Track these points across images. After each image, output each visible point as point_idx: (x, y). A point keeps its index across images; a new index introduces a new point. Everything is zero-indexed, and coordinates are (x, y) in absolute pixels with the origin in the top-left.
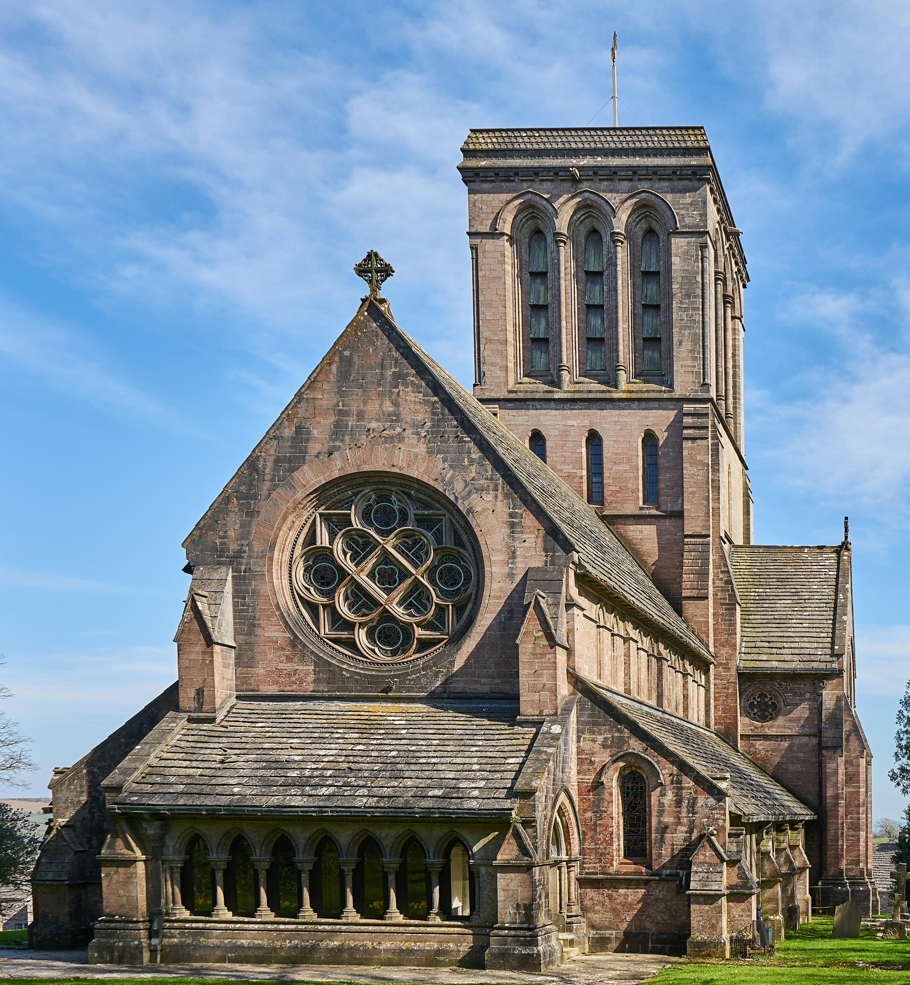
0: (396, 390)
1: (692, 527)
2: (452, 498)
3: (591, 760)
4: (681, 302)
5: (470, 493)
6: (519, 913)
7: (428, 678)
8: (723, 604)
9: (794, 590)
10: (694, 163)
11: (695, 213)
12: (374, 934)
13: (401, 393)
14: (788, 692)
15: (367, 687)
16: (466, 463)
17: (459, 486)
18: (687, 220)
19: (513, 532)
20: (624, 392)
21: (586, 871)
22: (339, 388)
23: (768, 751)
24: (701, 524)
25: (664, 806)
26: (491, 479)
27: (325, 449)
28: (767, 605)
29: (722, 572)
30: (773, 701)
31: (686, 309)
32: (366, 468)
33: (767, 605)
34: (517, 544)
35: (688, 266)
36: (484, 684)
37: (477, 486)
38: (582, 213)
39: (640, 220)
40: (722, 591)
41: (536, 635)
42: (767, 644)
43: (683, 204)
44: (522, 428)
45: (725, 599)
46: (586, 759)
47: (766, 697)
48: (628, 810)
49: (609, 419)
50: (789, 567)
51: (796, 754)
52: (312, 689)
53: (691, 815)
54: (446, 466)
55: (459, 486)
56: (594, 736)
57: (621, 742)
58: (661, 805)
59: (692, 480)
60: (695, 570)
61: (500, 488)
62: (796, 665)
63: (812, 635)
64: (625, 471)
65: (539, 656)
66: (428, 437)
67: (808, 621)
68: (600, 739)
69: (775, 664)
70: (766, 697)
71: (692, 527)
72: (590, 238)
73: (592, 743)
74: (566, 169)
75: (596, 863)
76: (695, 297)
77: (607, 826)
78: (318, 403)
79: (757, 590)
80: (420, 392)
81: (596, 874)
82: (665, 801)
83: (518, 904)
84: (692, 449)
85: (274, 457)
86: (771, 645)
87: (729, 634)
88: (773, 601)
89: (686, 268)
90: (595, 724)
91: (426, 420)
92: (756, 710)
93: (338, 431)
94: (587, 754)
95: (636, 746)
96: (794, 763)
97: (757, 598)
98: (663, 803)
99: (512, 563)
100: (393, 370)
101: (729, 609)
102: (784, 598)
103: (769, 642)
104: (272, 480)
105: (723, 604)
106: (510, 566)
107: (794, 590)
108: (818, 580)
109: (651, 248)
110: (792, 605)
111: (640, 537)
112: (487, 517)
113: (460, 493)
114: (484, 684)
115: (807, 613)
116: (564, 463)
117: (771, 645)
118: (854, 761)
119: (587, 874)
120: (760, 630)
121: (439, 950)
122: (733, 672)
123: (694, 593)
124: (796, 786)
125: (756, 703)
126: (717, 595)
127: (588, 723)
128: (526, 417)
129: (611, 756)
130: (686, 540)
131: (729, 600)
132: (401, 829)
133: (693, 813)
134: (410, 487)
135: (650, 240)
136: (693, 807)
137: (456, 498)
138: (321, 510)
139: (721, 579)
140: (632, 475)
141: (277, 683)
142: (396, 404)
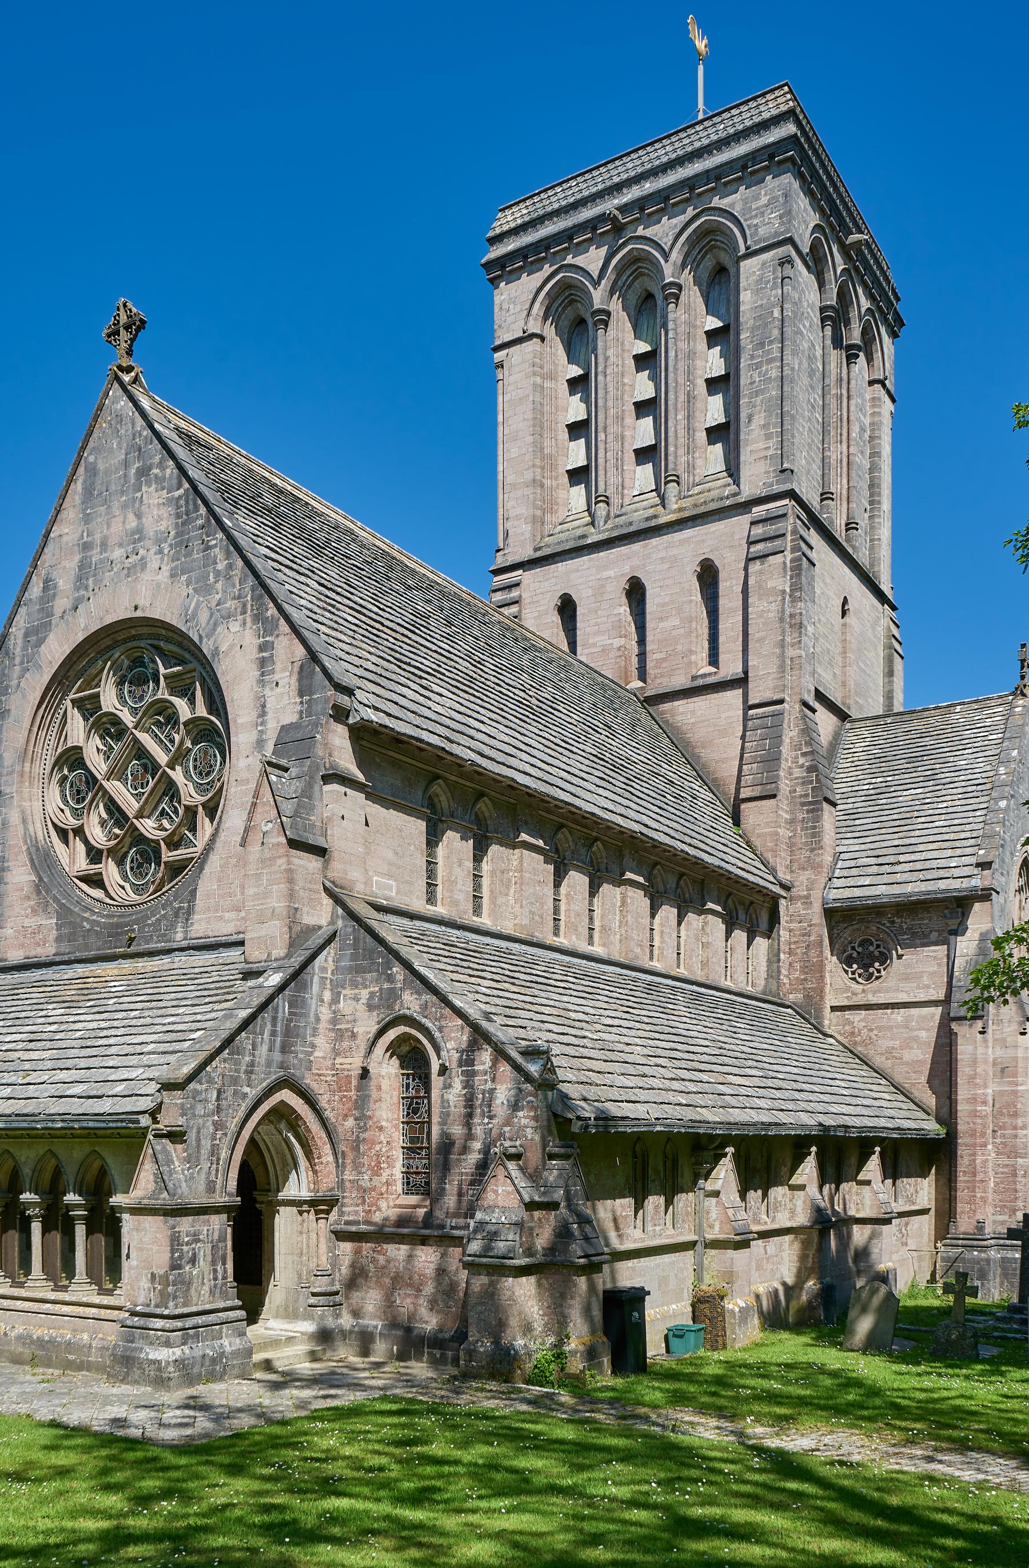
0: (139, 495)
1: (760, 691)
2: (196, 639)
3: (353, 1032)
4: (752, 357)
5: (215, 625)
6: (154, 1289)
7: (167, 920)
8: (803, 804)
9: (929, 773)
10: (771, 140)
11: (773, 215)
12: (8, 1313)
13: (144, 496)
14: (905, 933)
15: (106, 942)
16: (212, 580)
17: (203, 617)
18: (762, 231)
19: (263, 674)
20: (674, 512)
21: (346, 1218)
22: (84, 510)
23: (871, 1030)
24: (771, 686)
25: (449, 1106)
26: (239, 597)
27: (69, 606)
28: (884, 801)
29: (804, 754)
30: (882, 949)
31: (758, 366)
32: (109, 620)
33: (884, 801)
34: (267, 692)
35: (762, 299)
36: (229, 921)
37: (223, 613)
38: (628, 273)
39: (703, 257)
40: (803, 784)
41: (265, 829)
42: (873, 861)
43: (757, 208)
44: (548, 595)
45: (807, 795)
46: (347, 1030)
47: (872, 944)
48: (408, 1114)
49: (654, 557)
50: (928, 739)
51: (916, 1033)
52: (54, 951)
53: (486, 1120)
54: (191, 591)
55: (203, 617)
56: (357, 991)
57: (391, 996)
58: (445, 1103)
59: (759, 621)
60: (760, 756)
61: (249, 607)
62: (915, 888)
63: (946, 837)
64: (674, 628)
65: (268, 863)
66: (172, 552)
67: (943, 817)
68: (365, 994)
69: (881, 890)
70: (872, 944)
71: (760, 691)
72: (643, 308)
73: (354, 1003)
74: (602, 218)
75: (357, 1205)
76: (771, 342)
77: (373, 1143)
78: (65, 539)
79: (874, 781)
80: (163, 489)
81: (357, 1223)
82: (451, 1097)
83: (153, 1275)
84: (761, 572)
85: (23, 631)
86: (880, 860)
87: (812, 850)
88: (894, 794)
89: (760, 302)
90: (359, 970)
91: (170, 529)
92: (855, 966)
93: (85, 573)
94: (348, 1022)
95: (411, 1002)
96: (911, 1048)
97: (872, 792)
98: (448, 1101)
99: (262, 724)
100: (137, 465)
101: (812, 811)
102: (913, 786)
103: (878, 857)
104: (22, 663)
105: (803, 804)
106: (259, 728)
107: (929, 773)
108: (970, 751)
109: (720, 295)
110: (922, 796)
111: (692, 721)
112: (234, 657)
113: (204, 629)
114: (229, 921)
115: (945, 805)
116: (598, 633)
117: (880, 860)
118: (1009, 1039)
119: (347, 1223)
120: (868, 840)
121: (70, 1344)
122: (817, 908)
123: (757, 792)
124: (914, 1084)
125: (855, 955)
126: (795, 791)
127: (350, 970)
128: (554, 580)
129: (379, 1023)
130: (751, 712)
131: (813, 797)
132: (41, 1148)
133: (491, 1118)
134: (157, 637)
135: (720, 283)
136: (490, 1106)
137: (201, 637)
138: (72, 696)
139: (802, 766)
140: (682, 631)
141: (22, 946)
142: (139, 516)
